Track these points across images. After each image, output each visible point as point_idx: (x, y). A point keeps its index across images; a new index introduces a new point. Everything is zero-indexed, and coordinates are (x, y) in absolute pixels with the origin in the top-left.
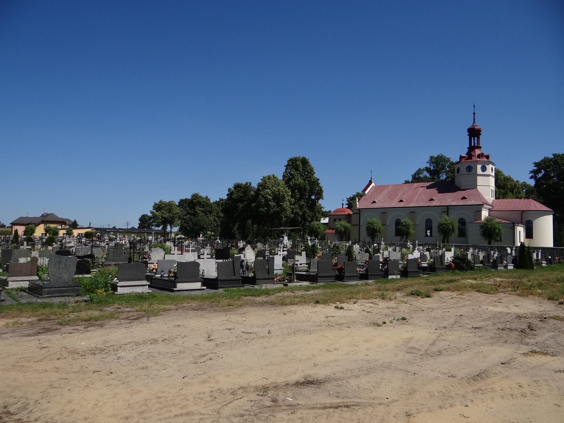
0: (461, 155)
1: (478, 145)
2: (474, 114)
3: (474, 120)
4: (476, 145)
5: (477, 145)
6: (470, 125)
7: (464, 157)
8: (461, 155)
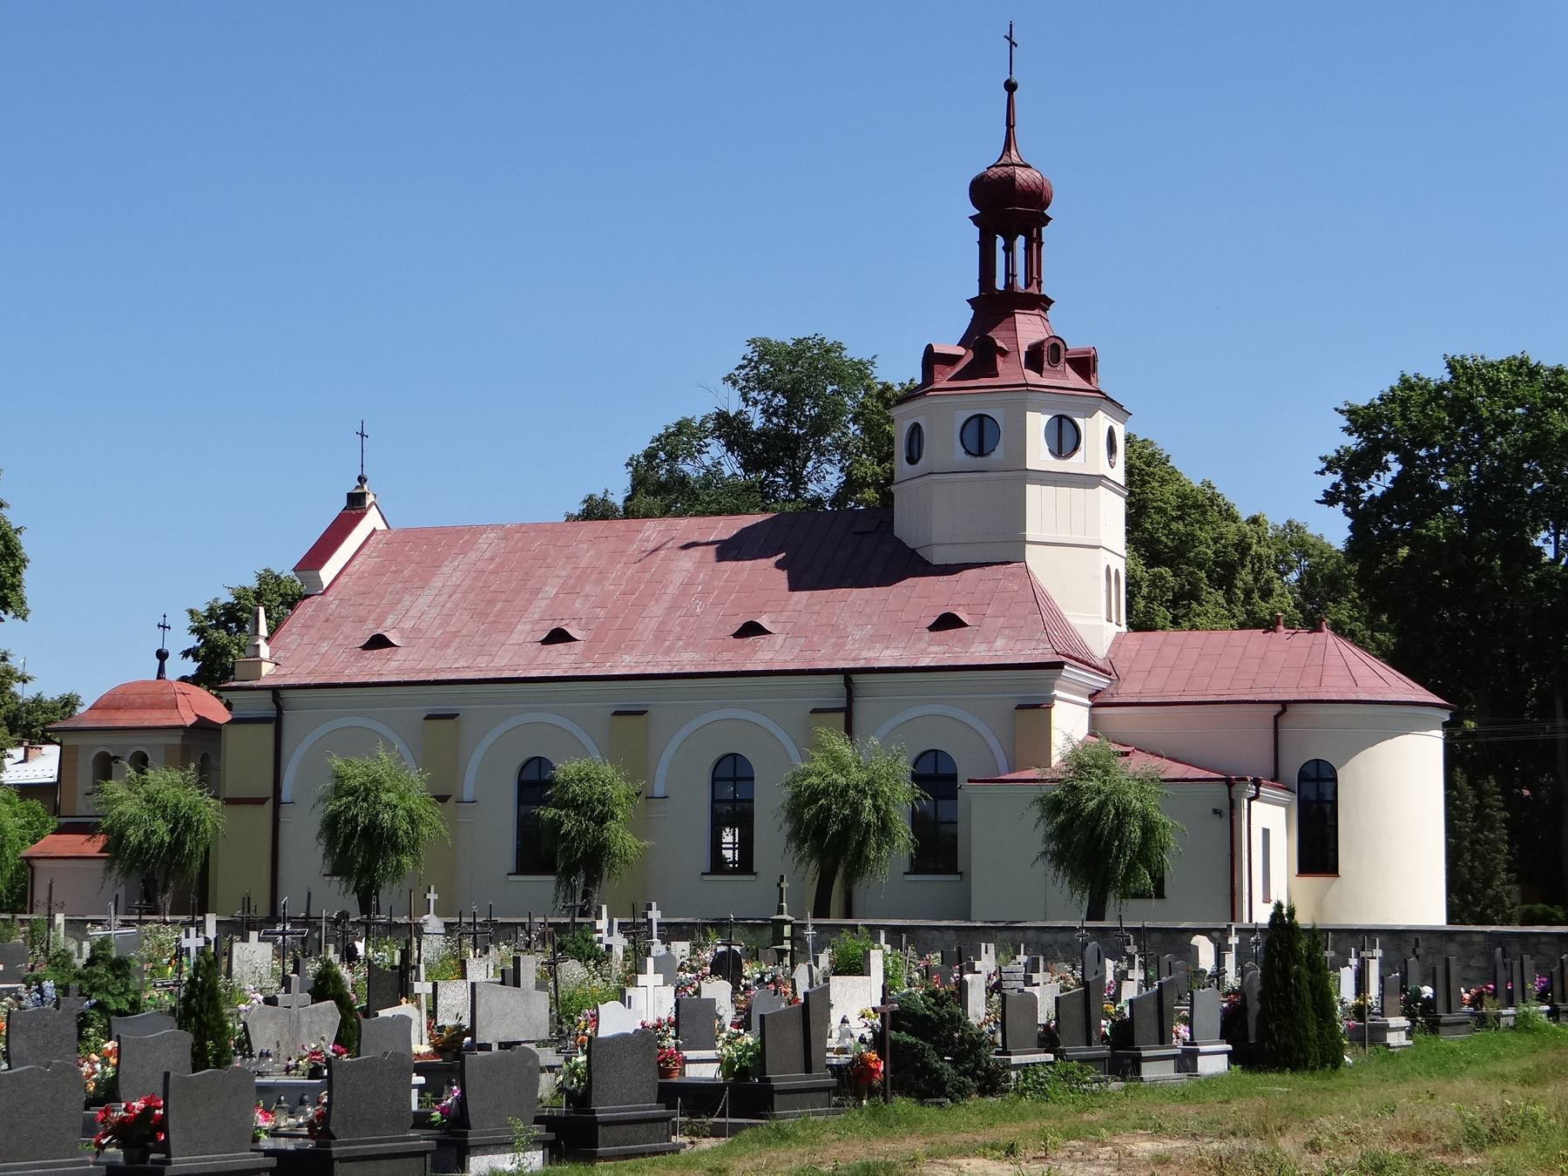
0: (929, 348)
1: (1033, 290)
2: (1010, 87)
3: (1010, 125)
4: (1020, 283)
5: (1027, 285)
6: (983, 158)
7: (951, 360)
8: (929, 348)
